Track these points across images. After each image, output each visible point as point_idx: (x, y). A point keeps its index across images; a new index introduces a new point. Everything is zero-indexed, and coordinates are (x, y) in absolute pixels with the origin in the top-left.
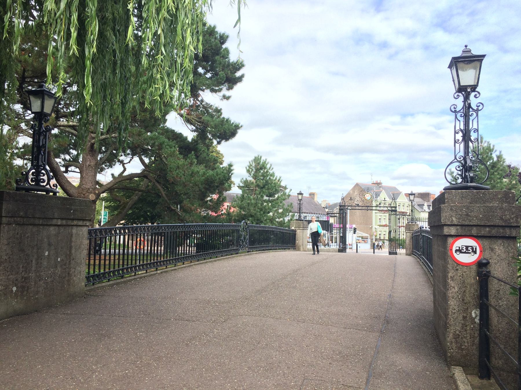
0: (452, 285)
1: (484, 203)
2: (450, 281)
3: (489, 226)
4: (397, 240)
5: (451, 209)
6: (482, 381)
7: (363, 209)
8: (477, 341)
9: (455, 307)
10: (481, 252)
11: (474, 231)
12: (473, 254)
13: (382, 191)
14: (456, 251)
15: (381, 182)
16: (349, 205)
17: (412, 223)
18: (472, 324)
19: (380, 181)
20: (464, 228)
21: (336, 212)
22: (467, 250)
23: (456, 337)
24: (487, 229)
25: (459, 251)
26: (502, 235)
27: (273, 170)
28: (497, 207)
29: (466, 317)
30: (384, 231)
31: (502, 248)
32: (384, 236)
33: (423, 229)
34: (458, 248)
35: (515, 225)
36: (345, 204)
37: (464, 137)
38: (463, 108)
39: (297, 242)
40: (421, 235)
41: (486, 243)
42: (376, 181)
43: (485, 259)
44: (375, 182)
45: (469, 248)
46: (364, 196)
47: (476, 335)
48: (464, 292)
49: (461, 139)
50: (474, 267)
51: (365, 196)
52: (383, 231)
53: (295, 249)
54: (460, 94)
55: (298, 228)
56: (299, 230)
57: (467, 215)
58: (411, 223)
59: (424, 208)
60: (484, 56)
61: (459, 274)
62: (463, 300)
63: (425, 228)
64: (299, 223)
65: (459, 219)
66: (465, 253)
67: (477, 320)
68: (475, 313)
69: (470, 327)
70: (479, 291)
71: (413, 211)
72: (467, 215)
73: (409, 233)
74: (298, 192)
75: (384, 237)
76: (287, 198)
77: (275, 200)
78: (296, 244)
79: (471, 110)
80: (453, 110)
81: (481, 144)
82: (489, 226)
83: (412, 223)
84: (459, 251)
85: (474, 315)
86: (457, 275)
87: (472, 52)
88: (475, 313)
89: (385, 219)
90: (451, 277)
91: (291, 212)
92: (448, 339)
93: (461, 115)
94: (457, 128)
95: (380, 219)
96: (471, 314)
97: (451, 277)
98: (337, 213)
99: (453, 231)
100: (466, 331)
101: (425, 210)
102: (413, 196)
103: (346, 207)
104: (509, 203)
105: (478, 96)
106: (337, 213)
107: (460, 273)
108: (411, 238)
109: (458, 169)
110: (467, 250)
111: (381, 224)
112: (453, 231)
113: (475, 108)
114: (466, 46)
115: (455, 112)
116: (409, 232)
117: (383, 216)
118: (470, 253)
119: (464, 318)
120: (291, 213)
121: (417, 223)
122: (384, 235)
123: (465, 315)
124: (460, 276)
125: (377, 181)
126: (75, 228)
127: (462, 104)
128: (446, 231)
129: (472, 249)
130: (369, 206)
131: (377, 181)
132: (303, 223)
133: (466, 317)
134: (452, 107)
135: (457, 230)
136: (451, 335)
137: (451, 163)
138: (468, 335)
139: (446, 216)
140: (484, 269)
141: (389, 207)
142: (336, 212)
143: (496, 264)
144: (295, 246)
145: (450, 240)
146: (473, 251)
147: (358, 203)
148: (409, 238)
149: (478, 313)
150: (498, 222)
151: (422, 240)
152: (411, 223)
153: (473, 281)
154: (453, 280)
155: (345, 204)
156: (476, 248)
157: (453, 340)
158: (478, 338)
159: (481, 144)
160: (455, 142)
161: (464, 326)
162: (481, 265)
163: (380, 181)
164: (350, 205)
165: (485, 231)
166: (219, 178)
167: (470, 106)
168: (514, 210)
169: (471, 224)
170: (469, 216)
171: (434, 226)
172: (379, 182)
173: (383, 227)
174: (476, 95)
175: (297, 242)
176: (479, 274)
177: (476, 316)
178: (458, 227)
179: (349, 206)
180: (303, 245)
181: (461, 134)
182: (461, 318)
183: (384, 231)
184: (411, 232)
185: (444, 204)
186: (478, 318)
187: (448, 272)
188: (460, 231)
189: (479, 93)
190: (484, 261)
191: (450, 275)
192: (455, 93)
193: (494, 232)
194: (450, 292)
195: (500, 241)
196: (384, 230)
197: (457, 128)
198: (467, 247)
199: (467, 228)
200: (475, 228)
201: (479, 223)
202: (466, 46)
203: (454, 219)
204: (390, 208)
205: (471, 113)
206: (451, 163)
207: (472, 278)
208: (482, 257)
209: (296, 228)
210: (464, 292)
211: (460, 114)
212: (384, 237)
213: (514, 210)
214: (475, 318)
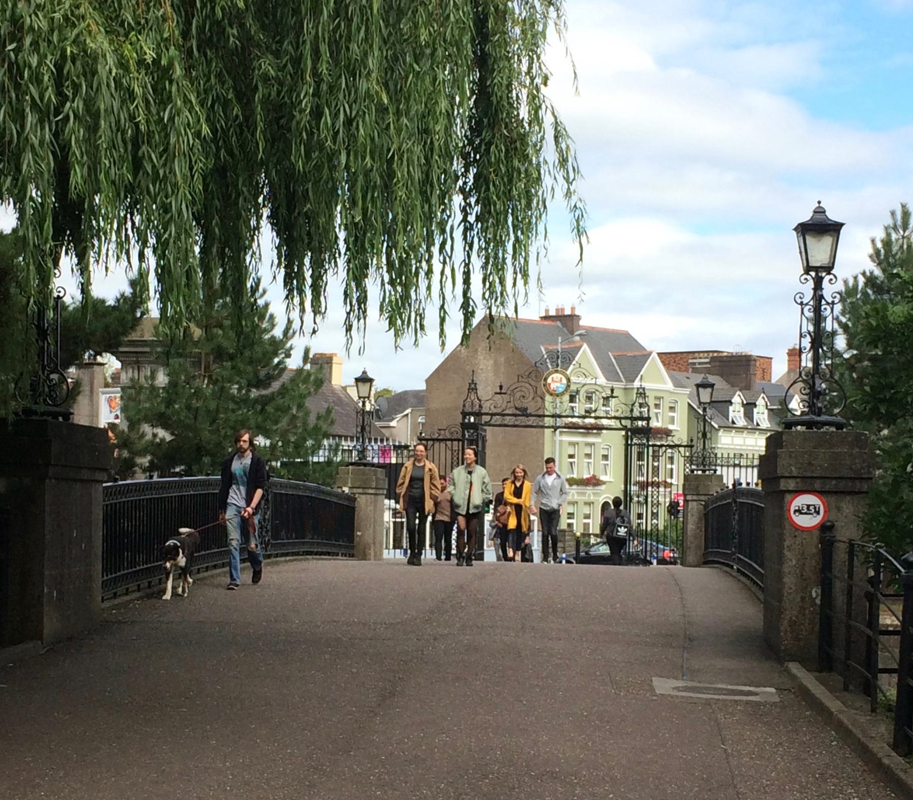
0: (789, 557)
1: (831, 448)
2: (786, 552)
3: (836, 478)
4: (651, 534)
5: (790, 456)
6: (822, 674)
7: (530, 423)
8: (817, 628)
9: (793, 586)
10: (825, 512)
11: (817, 485)
12: (815, 515)
13: (579, 348)
14: (795, 511)
15: (577, 313)
16: (495, 411)
17: (704, 471)
18: (812, 606)
19: (573, 309)
20: (805, 480)
21: (452, 433)
22: (809, 510)
23: (792, 624)
24: (834, 482)
25: (799, 511)
26: (850, 490)
27: (266, 297)
28: (846, 452)
29: (805, 597)
30: (586, 503)
31: (850, 506)
32: (570, 521)
33: (739, 487)
34: (797, 508)
35: (866, 476)
36: (480, 406)
37: (813, 342)
38: (812, 298)
39: (359, 533)
40: (736, 502)
41: (832, 499)
42: (557, 310)
43: (829, 521)
44: (552, 313)
45: (811, 508)
46: (546, 379)
47: (817, 620)
48: (804, 564)
49: (808, 346)
50: (816, 533)
51: (549, 380)
52: (581, 504)
53: (352, 556)
54: (809, 277)
55: (360, 491)
56: (363, 496)
57: (810, 464)
58: (700, 472)
59: (731, 414)
60: (842, 225)
61: (797, 543)
62: (802, 575)
63: (744, 485)
64: (364, 474)
65: (799, 468)
66: (806, 513)
67: (818, 601)
68: (815, 592)
69: (810, 611)
70: (821, 563)
71: (709, 435)
72: (810, 464)
73: (695, 503)
74: (359, 374)
75: (586, 526)
76: (312, 390)
77: (271, 398)
78: (357, 539)
79: (823, 302)
80: (799, 301)
81: (904, 231)
82: (836, 478)
83: (704, 471)
84: (799, 511)
85: (814, 595)
86: (795, 543)
87: (827, 213)
88: (816, 591)
89: (588, 456)
90: (788, 547)
91: (327, 436)
92: (782, 628)
93: (810, 309)
94: (804, 330)
95: (571, 456)
96: (811, 592)
97: (788, 547)
98: (452, 440)
99: (792, 485)
100: (804, 615)
101: (733, 422)
102: (709, 390)
103: (486, 418)
104: (860, 448)
105: (834, 280)
106: (452, 440)
107: (799, 540)
108: (700, 519)
109: (803, 392)
110: (809, 510)
111: (575, 476)
112: (792, 485)
113: (830, 301)
114: (819, 202)
115: (802, 304)
116: (695, 498)
117: (582, 446)
118: (811, 514)
119: (803, 598)
120: (328, 438)
121: (718, 473)
122: (587, 517)
123: (804, 595)
124: (799, 545)
125: (563, 310)
126: (78, 486)
127: (812, 292)
128: (783, 485)
129: (815, 508)
130: (560, 416)
131: (563, 310)
132: (375, 472)
133: (805, 597)
134: (798, 296)
135: (797, 483)
136: (786, 623)
137: (795, 382)
138: (807, 621)
139: (786, 465)
140: (828, 534)
141: (626, 418)
142: (449, 437)
143: (842, 527)
144: (353, 548)
145: (788, 497)
146: (815, 511)
147: (525, 406)
148: (695, 518)
149: (819, 592)
150: (845, 473)
151: (736, 517)
152: (700, 472)
153: (814, 551)
154: (789, 550)
155: (480, 406)
156: (819, 508)
157: (788, 629)
158: (818, 625)
159: (904, 231)
160: (801, 336)
161: (803, 608)
162: (825, 528)
163: (573, 309)
164: (499, 411)
165: (831, 485)
166: (107, 327)
167: (822, 297)
168: (865, 456)
169: (814, 475)
170: (813, 465)
171: (768, 479)
172: (568, 312)
173: (581, 489)
174: (831, 280)
175: (359, 533)
176: (822, 541)
177: (817, 596)
178: (798, 480)
179: (492, 415)
180: (374, 543)
181: (808, 339)
182: (799, 599)
183: (586, 503)
184: (703, 498)
185: (781, 448)
186: (819, 598)
187: (785, 541)
188: (801, 486)
189: (836, 277)
190: (829, 524)
191: (787, 543)
192: (802, 275)
193: (842, 485)
194: (787, 566)
195: (848, 498)
196: (586, 498)
197: (804, 330)
198: (808, 506)
199: (809, 481)
200: (818, 481)
201: (823, 474)
202: (819, 202)
203: (793, 469)
204: (629, 421)
205: (823, 308)
206: (795, 382)
207: (813, 547)
208: (826, 519)
209: (355, 491)
210: (804, 564)
211: (808, 307)
212: (586, 526)
213: (865, 456)
214: (816, 598)
